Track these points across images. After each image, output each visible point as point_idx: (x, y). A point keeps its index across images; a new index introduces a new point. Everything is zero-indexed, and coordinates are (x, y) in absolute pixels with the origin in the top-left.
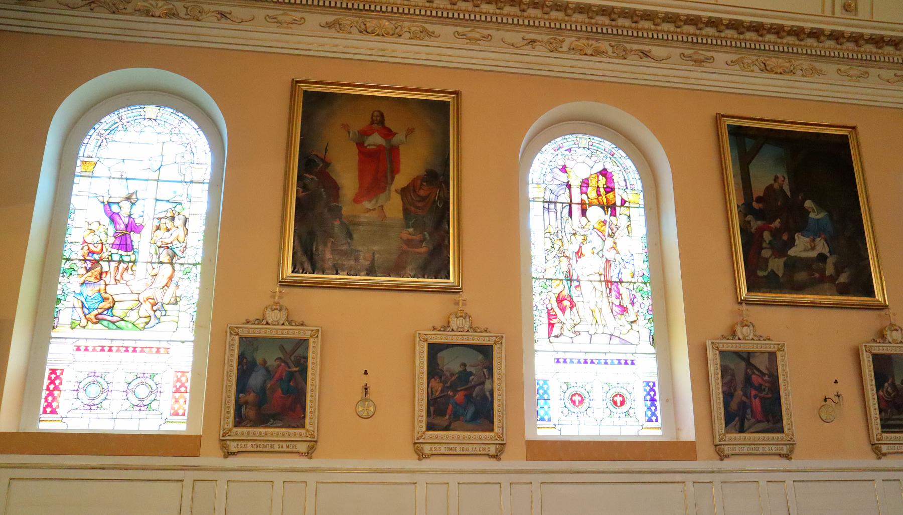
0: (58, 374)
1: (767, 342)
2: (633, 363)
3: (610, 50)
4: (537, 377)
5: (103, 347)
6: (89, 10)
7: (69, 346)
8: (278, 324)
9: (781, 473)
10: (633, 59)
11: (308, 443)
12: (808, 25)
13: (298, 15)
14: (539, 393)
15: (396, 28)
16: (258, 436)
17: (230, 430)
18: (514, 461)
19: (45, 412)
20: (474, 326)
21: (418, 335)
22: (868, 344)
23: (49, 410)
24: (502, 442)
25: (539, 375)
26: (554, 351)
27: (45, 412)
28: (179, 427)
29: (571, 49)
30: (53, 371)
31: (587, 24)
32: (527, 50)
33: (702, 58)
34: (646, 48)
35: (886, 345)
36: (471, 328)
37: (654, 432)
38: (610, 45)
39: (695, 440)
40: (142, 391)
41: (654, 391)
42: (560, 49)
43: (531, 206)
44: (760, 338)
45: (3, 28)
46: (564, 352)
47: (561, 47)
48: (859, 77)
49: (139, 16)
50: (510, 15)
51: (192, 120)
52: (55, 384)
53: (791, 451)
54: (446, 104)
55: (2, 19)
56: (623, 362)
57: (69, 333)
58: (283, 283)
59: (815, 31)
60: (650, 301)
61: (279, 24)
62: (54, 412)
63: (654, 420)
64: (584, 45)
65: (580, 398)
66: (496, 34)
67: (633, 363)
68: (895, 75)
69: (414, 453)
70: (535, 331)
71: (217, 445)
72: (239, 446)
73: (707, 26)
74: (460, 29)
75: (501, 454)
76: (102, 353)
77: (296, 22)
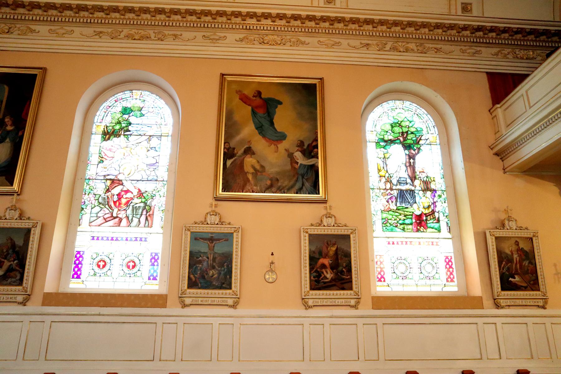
0: (81, 254)
1: (526, 231)
5: (136, 238)
6: (99, 38)
7: (88, 236)
8: (214, 224)
9: (247, 318)
11: (355, 300)
12: (362, 17)
13: (69, 29)
15: (282, 40)
16: (339, 296)
17: (355, 292)
18: (365, 310)
19: (73, 277)
20: (338, 222)
21: (302, 229)
22: (492, 231)
23: (75, 276)
24: (359, 297)
27: (73, 277)
28: (153, 287)
29: (128, 37)
30: (79, 252)
31: (105, 19)
32: (364, 50)
33: (217, 38)
35: (505, 231)
36: (336, 223)
37: (452, 288)
38: (154, 33)
39: (480, 295)
41: (451, 262)
42: (119, 37)
43: (368, 145)
44: (521, 228)
45: (2, 48)
46: (98, 232)
47: (120, 36)
50: (85, 17)
51: (422, 108)
52: (79, 260)
53: (546, 303)
54: (315, 85)
57: (89, 229)
58: (217, 199)
59: (467, 26)
61: (57, 35)
62: (78, 277)
63: (383, 281)
65: (104, 263)
66: (344, 42)
67: (146, 241)
68: (361, 44)
69: (179, 303)
70: (80, 218)
71: (177, 300)
72: (194, 301)
73: (462, 30)
74: (53, 28)
75: (358, 305)
76: (93, 241)
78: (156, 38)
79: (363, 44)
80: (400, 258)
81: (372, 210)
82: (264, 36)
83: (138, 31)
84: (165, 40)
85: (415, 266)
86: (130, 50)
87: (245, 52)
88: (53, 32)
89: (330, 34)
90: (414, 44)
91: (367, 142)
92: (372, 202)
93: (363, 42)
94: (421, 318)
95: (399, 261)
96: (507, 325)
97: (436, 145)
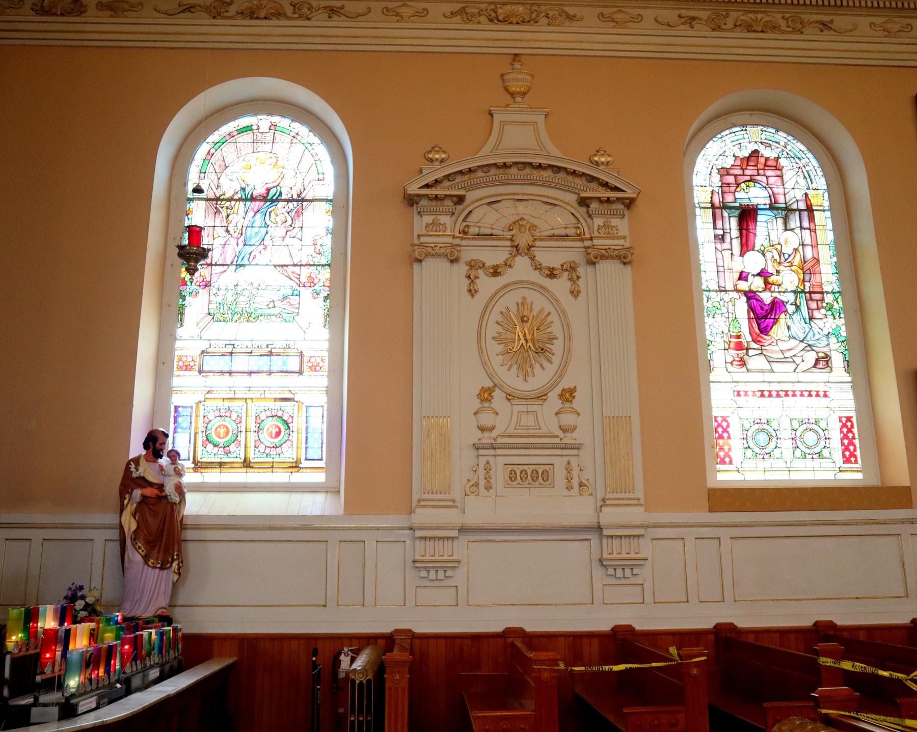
2: (825, 396)
3: (783, 24)
4: (714, 414)
7: (729, 389)
10: (810, 32)
13: (635, 12)
14: (723, 430)
25: (717, 411)
26: (733, 382)
32: (684, 30)
34: (826, 18)
37: (853, 475)
38: (783, 18)
39: (909, 485)
40: (810, 438)
42: (226, 14)
46: (745, 382)
47: (725, 24)
48: (900, 31)
49: (243, 19)
55: (2, 33)
56: (814, 394)
60: (843, 321)
64: (752, 19)
67: (825, 396)
68: (680, 16)
70: (709, 358)
77: (419, 14)
78: (790, 29)
79: (683, 17)
80: (759, 421)
81: (708, 333)
82: (499, 6)
83: (756, 15)
84: (313, 19)
85: (786, 434)
86: (103, 36)
87: (308, 36)
88: (606, 20)
89: (906, 9)
90: (779, 16)
91: (696, 207)
92: (706, 319)
93: (684, 13)
94: (81, 538)
95: (757, 426)
96: (740, 542)
97: (824, 211)
